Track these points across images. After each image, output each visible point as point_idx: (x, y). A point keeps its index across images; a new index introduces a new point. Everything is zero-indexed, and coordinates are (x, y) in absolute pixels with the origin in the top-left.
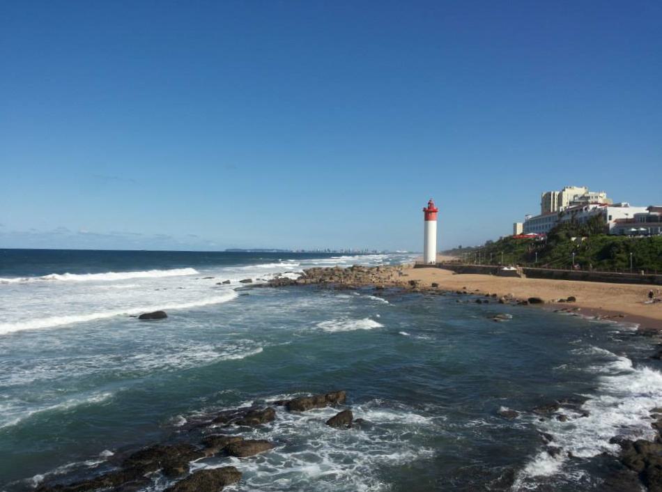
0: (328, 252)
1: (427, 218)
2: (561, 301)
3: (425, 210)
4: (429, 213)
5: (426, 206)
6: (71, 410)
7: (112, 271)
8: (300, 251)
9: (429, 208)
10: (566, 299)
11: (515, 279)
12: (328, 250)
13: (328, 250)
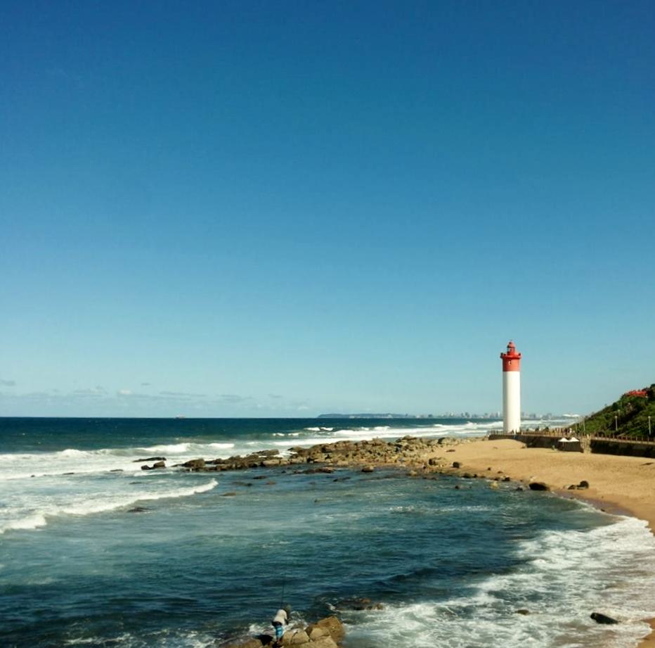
0: (466, 417)
1: (506, 369)
2: (572, 487)
3: (503, 356)
4: (508, 359)
5: (505, 351)
6: (392, 599)
7: (71, 448)
8: (426, 417)
9: (509, 353)
10: (579, 484)
11: (577, 454)
12: (466, 414)
13: (466, 414)
